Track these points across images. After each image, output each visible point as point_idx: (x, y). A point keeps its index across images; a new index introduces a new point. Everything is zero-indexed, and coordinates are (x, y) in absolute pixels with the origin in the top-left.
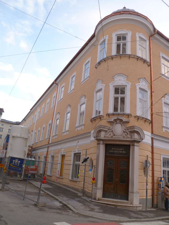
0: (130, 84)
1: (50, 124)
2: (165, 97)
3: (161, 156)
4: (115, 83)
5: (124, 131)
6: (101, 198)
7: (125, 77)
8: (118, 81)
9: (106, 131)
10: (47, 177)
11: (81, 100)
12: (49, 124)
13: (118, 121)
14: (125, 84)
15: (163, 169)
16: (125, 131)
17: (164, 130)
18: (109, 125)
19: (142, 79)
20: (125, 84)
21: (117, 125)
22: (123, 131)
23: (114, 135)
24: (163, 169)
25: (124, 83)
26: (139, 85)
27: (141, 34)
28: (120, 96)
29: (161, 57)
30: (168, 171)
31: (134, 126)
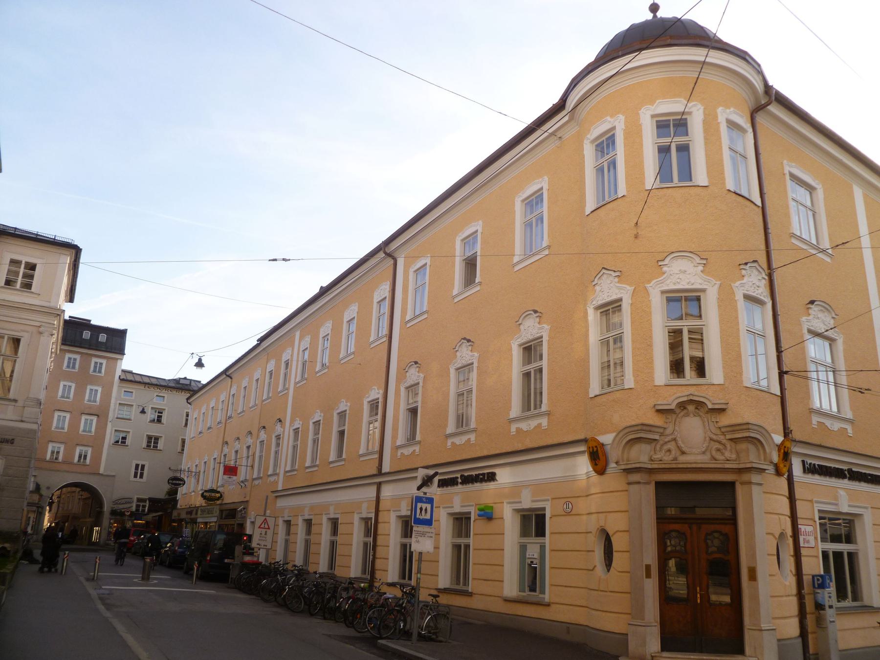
0: (717, 287)
1: (374, 405)
2: (810, 311)
3: (815, 505)
4: (668, 282)
5: (711, 439)
7: (698, 260)
10: (384, 589)
11: (522, 327)
12: (370, 399)
13: (691, 408)
15: (822, 546)
16: (714, 437)
17: (815, 419)
18: (656, 420)
19: (749, 265)
21: (687, 419)
22: (708, 439)
23: (683, 453)
24: (822, 546)
26: (743, 285)
27: (732, 109)
29: (788, 177)
30: (834, 552)
31: (748, 423)
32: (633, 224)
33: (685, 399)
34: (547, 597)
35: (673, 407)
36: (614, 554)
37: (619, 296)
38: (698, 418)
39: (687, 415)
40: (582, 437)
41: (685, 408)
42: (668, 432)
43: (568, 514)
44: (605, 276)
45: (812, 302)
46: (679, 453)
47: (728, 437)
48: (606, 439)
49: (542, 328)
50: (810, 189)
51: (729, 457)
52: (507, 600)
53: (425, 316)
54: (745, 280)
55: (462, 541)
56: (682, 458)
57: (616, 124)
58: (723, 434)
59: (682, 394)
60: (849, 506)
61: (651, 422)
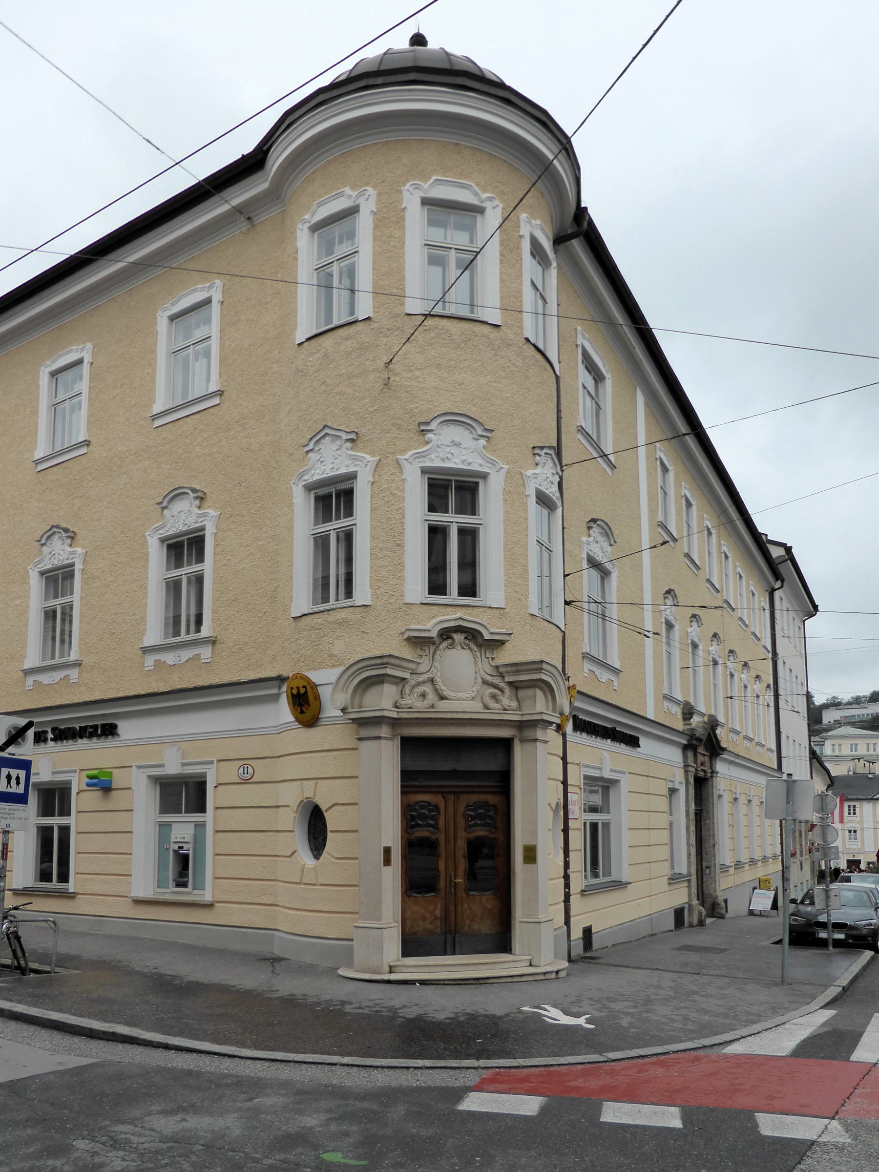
0: (503, 472)
2: (591, 531)
4: (433, 456)
6: (398, 960)
8: (448, 449)
9: (404, 679)
13: (458, 637)
14: (481, 465)
16: (489, 679)
18: (406, 652)
19: (545, 451)
20: (481, 469)
22: (480, 680)
23: (442, 698)
25: (476, 464)
28: (453, 520)
31: (542, 662)
32: (381, 364)
34: (207, 896)
35: (434, 634)
36: (329, 835)
37: (352, 469)
38: (468, 652)
39: (452, 646)
40: (274, 674)
41: (449, 637)
42: (423, 668)
43: (246, 782)
44: (328, 439)
45: (594, 521)
46: (436, 698)
47: (507, 679)
48: (324, 677)
49: (205, 515)
50: (598, 377)
51: (507, 707)
52: (138, 902)
54: (538, 470)
55: (55, 821)
56: (443, 705)
57: (361, 201)
58: (502, 676)
60: (612, 771)
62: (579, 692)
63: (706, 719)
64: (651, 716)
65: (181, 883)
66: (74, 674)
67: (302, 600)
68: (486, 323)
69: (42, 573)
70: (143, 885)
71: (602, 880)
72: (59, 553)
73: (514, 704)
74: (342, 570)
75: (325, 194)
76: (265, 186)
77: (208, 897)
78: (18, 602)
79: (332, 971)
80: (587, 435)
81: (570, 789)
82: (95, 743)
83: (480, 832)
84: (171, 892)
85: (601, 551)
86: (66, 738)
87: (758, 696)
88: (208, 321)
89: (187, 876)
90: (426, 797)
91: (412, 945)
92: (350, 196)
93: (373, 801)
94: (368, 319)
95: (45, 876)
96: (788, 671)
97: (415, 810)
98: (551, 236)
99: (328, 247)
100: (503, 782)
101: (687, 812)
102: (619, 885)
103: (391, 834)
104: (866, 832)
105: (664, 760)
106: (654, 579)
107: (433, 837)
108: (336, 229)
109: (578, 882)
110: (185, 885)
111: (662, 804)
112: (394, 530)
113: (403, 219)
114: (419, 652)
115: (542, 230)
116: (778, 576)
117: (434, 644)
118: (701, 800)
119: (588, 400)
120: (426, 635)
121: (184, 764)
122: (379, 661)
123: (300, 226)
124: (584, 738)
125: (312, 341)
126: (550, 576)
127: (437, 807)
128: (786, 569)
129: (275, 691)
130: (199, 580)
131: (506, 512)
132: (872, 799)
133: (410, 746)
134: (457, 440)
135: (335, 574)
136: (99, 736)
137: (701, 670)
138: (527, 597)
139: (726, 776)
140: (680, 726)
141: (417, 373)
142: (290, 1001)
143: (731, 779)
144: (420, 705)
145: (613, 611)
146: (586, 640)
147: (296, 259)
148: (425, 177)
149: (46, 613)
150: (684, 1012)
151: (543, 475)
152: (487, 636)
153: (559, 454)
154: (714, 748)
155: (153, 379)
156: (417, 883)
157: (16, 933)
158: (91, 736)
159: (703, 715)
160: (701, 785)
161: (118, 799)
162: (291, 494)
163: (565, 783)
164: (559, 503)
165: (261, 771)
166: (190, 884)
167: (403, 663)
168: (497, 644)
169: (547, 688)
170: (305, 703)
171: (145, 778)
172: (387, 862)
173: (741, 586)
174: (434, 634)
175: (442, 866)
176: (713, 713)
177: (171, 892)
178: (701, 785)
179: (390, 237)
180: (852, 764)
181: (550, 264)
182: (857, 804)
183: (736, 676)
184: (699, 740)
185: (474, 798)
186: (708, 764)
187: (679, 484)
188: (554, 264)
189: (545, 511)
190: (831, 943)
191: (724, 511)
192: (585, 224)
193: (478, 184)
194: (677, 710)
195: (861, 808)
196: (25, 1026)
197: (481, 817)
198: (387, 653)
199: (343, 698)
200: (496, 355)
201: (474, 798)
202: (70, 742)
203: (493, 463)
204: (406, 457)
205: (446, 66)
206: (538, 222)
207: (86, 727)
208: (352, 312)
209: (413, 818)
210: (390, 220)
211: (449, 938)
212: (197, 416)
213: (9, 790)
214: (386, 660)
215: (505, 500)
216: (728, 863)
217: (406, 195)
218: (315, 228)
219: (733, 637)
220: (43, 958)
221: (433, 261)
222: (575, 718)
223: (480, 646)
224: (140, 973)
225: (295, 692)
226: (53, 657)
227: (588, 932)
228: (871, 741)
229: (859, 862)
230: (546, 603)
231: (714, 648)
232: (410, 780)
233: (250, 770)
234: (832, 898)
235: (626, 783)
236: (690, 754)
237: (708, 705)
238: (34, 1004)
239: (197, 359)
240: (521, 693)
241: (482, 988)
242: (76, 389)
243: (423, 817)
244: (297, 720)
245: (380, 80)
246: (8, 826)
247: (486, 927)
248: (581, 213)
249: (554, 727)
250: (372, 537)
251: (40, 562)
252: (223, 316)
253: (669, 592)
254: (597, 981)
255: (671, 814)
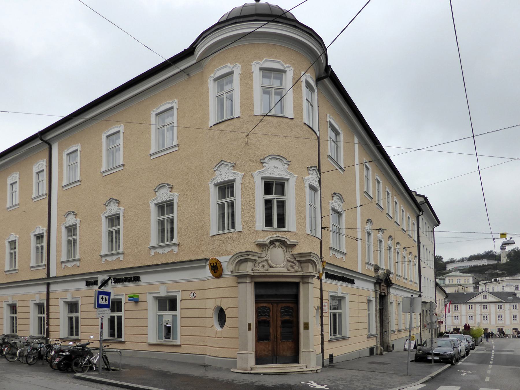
0: (295, 178)
4: (266, 172)
13: (277, 244)
16: (290, 259)
18: (257, 250)
22: (286, 260)
23: (271, 267)
25: (284, 175)
31: (311, 253)
33: (275, 239)
34: (123, 339)
35: (267, 242)
36: (227, 319)
37: (233, 178)
39: (275, 247)
40: (203, 257)
41: (273, 244)
42: (263, 256)
43: (193, 299)
45: (335, 194)
46: (268, 267)
47: (299, 259)
48: (224, 259)
50: (337, 133)
51: (297, 270)
52: (150, 345)
53: (79, 183)
54: (310, 176)
56: (271, 270)
57: (235, 69)
58: (295, 258)
59: (274, 236)
60: (342, 293)
61: (253, 250)
62: (327, 263)
63: (385, 271)
64: (360, 271)
65: (168, 337)
66: (121, 257)
67: (214, 229)
68: (287, 118)
69: (106, 217)
70: (153, 338)
71: (338, 336)
72: (113, 209)
73: (300, 269)
74: (230, 211)
75: (220, 66)
76: (195, 61)
77: (179, 343)
78: (97, 228)
79: (229, 370)
80: (332, 159)
81: (324, 301)
82: (131, 284)
83: (287, 318)
84: (163, 341)
85: (337, 205)
86: (119, 282)
87: (410, 261)
88: (172, 115)
89: (170, 335)
90: (265, 305)
91: (259, 360)
92: (230, 67)
93: (244, 306)
94: (239, 117)
95: (112, 335)
96: (425, 249)
97: (261, 310)
98: (315, 80)
99: (221, 87)
100: (296, 299)
101: (376, 309)
102: (345, 338)
103: (251, 318)
104: (462, 317)
105: (367, 289)
106: (362, 215)
107: (268, 320)
108: (225, 80)
109: (327, 337)
110: (169, 338)
111: (365, 306)
112: (251, 202)
113: (252, 76)
114: (261, 249)
115: (311, 77)
116: (420, 210)
117: (267, 246)
118: (383, 304)
119: (333, 143)
120: (264, 243)
121: (168, 292)
122: (245, 253)
123: (209, 79)
124: (330, 281)
125: (216, 126)
126: (315, 218)
127: (269, 309)
128: (425, 207)
129: (204, 264)
130: (172, 221)
131: (296, 194)
132: (465, 303)
133: (258, 285)
134: (276, 166)
135: (227, 216)
136: (133, 281)
137: (383, 252)
138: (305, 227)
139: (395, 296)
140: (373, 274)
141: (259, 139)
142: (213, 380)
143: (396, 295)
144: (262, 270)
145: (343, 231)
146: (331, 242)
147: (208, 92)
148: (261, 59)
149: (109, 233)
150: (365, 384)
151: (312, 178)
152: (289, 243)
153: (319, 170)
154: (388, 283)
155: (150, 139)
156: (261, 337)
157: (105, 356)
158: (129, 281)
159: (384, 270)
160: (383, 299)
161: (141, 305)
162: (209, 187)
163: (321, 299)
164: (319, 189)
165: (199, 295)
166: (171, 338)
167: (255, 254)
168: (293, 246)
169: (313, 263)
170: (216, 269)
171: (152, 298)
172: (250, 329)
173: (404, 217)
174: (267, 242)
175: (271, 331)
176: (389, 269)
177: (163, 341)
178: (383, 299)
179: (247, 84)
180: (457, 288)
181: (314, 91)
182: (459, 305)
183: (400, 253)
184: (382, 280)
185: (284, 305)
186: (386, 290)
187: (374, 174)
188: (316, 91)
189: (313, 192)
190: (433, 361)
191: (395, 184)
192: (330, 72)
193: (283, 61)
194: (372, 268)
195: (461, 307)
196: (115, 387)
197: (286, 312)
198: (248, 250)
199: (232, 267)
200: (291, 130)
201: (284, 305)
202: (121, 284)
203: (291, 174)
204: (256, 173)
205: (268, 12)
206: (309, 75)
207: (127, 278)
208: (232, 114)
209: (260, 312)
210: (247, 76)
211: (274, 358)
212: (169, 155)
213: (103, 303)
214: (248, 253)
215: (296, 189)
216: (394, 330)
217: (253, 67)
218: (215, 80)
219: (398, 236)
220: (115, 365)
221: (265, 92)
222: (326, 273)
223: (286, 247)
224: (154, 370)
225: (212, 265)
226: (112, 250)
227: (331, 356)
228: (467, 278)
229: (459, 329)
230: (313, 228)
231: (390, 242)
232: (258, 298)
233: (195, 294)
234: (434, 343)
235: (348, 298)
236: (378, 286)
237: (386, 265)
238: (116, 380)
239: (168, 131)
240: (303, 265)
241: (287, 376)
242: (117, 143)
243: (264, 312)
244: (213, 275)
245: (241, 20)
246: (103, 316)
247: (288, 353)
248: (328, 68)
249: (316, 277)
250: (242, 205)
251: (106, 213)
252: (178, 114)
253: (369, 220)
254: (332, 374)
255: (369, 310)
